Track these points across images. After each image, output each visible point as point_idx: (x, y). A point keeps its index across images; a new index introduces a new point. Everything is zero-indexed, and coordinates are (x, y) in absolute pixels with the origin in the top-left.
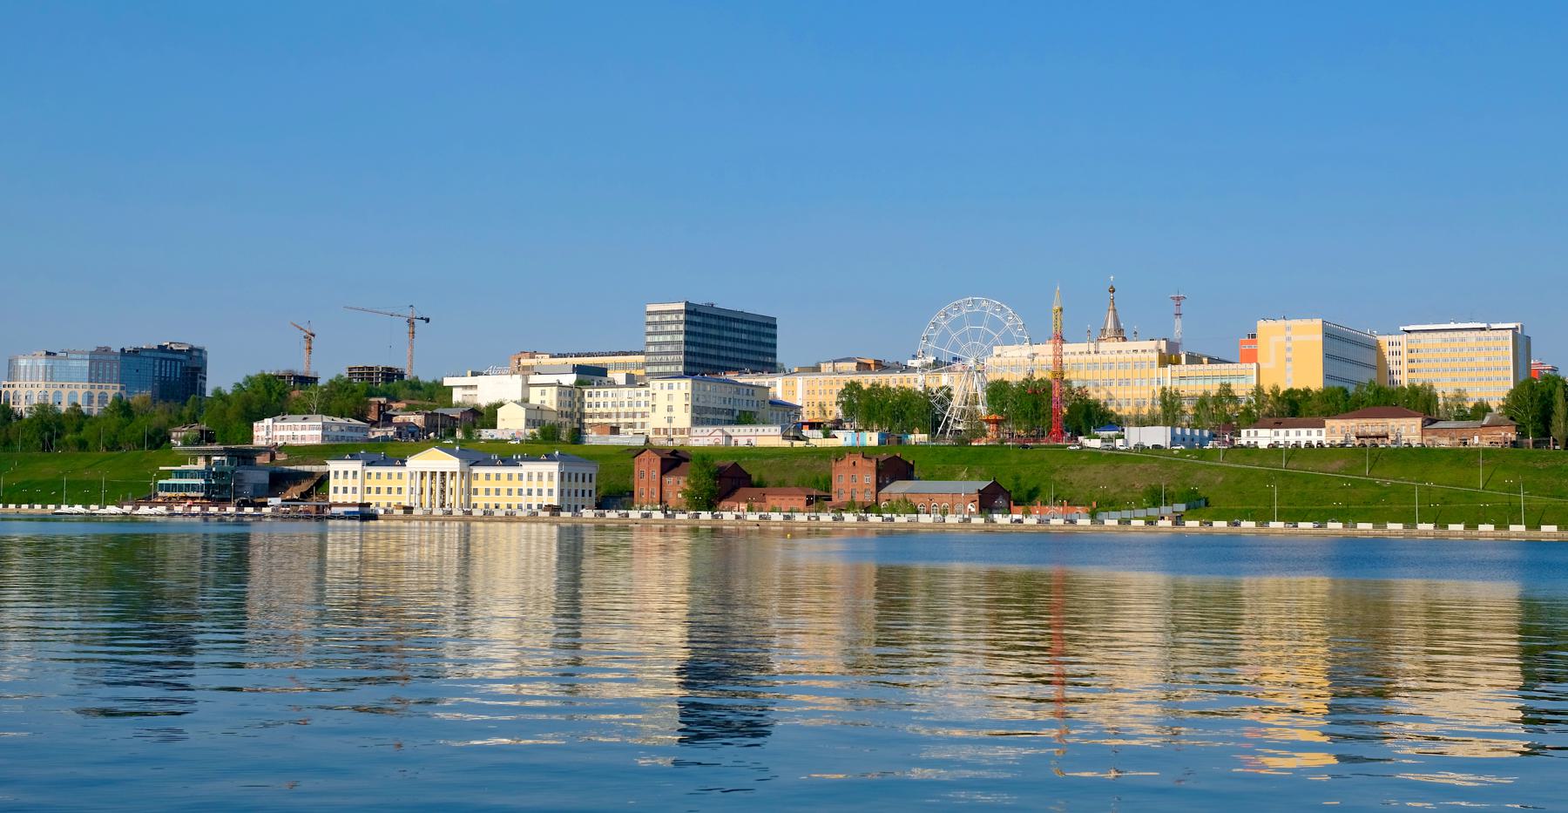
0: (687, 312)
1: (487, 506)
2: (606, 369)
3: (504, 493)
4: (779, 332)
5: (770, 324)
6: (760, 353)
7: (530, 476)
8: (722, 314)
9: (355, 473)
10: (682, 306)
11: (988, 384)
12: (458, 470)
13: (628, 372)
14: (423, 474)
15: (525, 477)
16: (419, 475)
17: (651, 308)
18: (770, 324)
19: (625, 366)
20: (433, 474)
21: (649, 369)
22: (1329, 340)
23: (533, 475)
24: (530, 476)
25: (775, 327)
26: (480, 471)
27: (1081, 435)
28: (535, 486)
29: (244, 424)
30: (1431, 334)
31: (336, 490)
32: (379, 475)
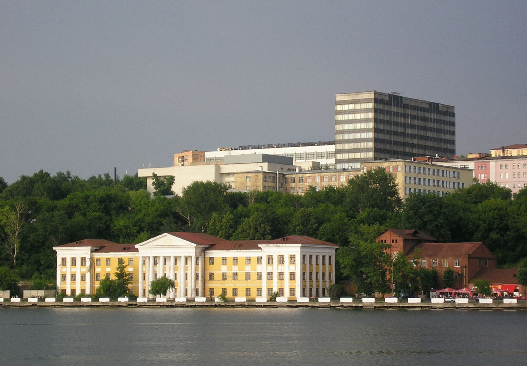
0: (376, 101)
1: (224, 291)
2: (292, 159)
3: (241, 276)
4: (458, 120)
5: (449, 112)
6: (390, 142)
7: (270, 260)
8: (419, 105)
9: (83, 260)
10: (372, 96)
11: (121, 199)
12: (193, 255)
13: (314, 160)
14: (155, 260)
15: (265, 260)
16: (152, 260)
17: (339, 98)
18: (449, 112)
19: (308, 156)
20: (155, 259)
21: (339, 157)
22: (490, 153)
23: (285, 257)
24: (270, 260)
25: (453, 115)
26: (216, 254)
27: (53, 247)
28: (276, 268)
29: (506, 187)
30: (253, 164)
31: (64, 277)
32: (108, 260)
